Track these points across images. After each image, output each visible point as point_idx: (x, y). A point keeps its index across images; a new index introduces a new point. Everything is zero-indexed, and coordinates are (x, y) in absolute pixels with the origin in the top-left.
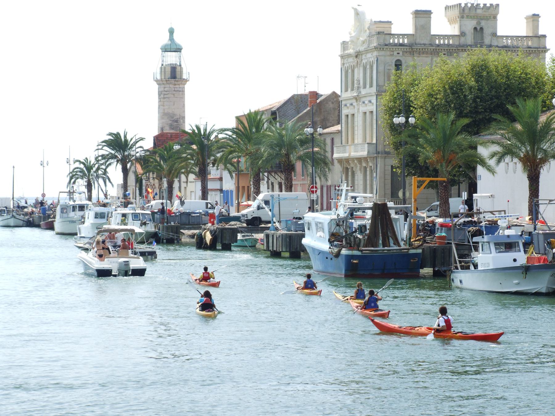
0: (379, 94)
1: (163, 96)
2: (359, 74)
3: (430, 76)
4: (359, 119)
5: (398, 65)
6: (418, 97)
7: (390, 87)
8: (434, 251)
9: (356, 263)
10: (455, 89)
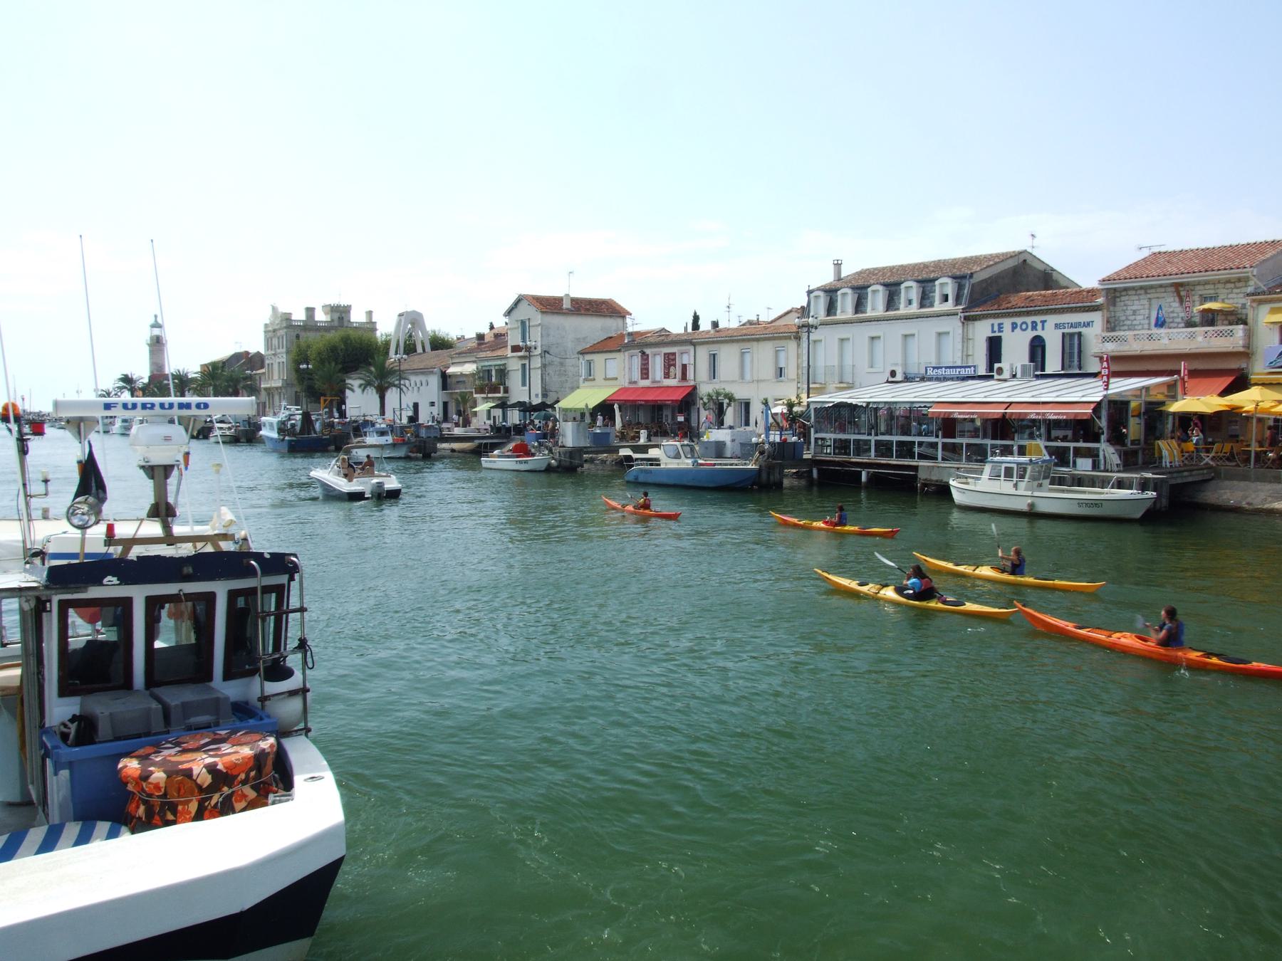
0: (287, 353)
1: (152, 353)
2: (275, 342)
3: (317, 342)
4: (276, 367)
5: (298, 337)
6: (312, 354)
7: (294, 349)
8: (335, 437)
9: (795, 443)
10: (333, 349)
